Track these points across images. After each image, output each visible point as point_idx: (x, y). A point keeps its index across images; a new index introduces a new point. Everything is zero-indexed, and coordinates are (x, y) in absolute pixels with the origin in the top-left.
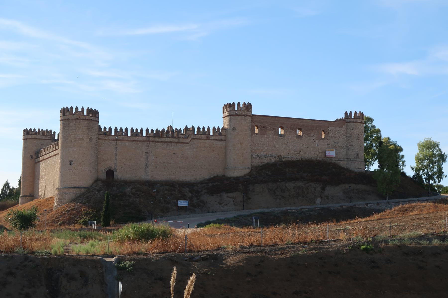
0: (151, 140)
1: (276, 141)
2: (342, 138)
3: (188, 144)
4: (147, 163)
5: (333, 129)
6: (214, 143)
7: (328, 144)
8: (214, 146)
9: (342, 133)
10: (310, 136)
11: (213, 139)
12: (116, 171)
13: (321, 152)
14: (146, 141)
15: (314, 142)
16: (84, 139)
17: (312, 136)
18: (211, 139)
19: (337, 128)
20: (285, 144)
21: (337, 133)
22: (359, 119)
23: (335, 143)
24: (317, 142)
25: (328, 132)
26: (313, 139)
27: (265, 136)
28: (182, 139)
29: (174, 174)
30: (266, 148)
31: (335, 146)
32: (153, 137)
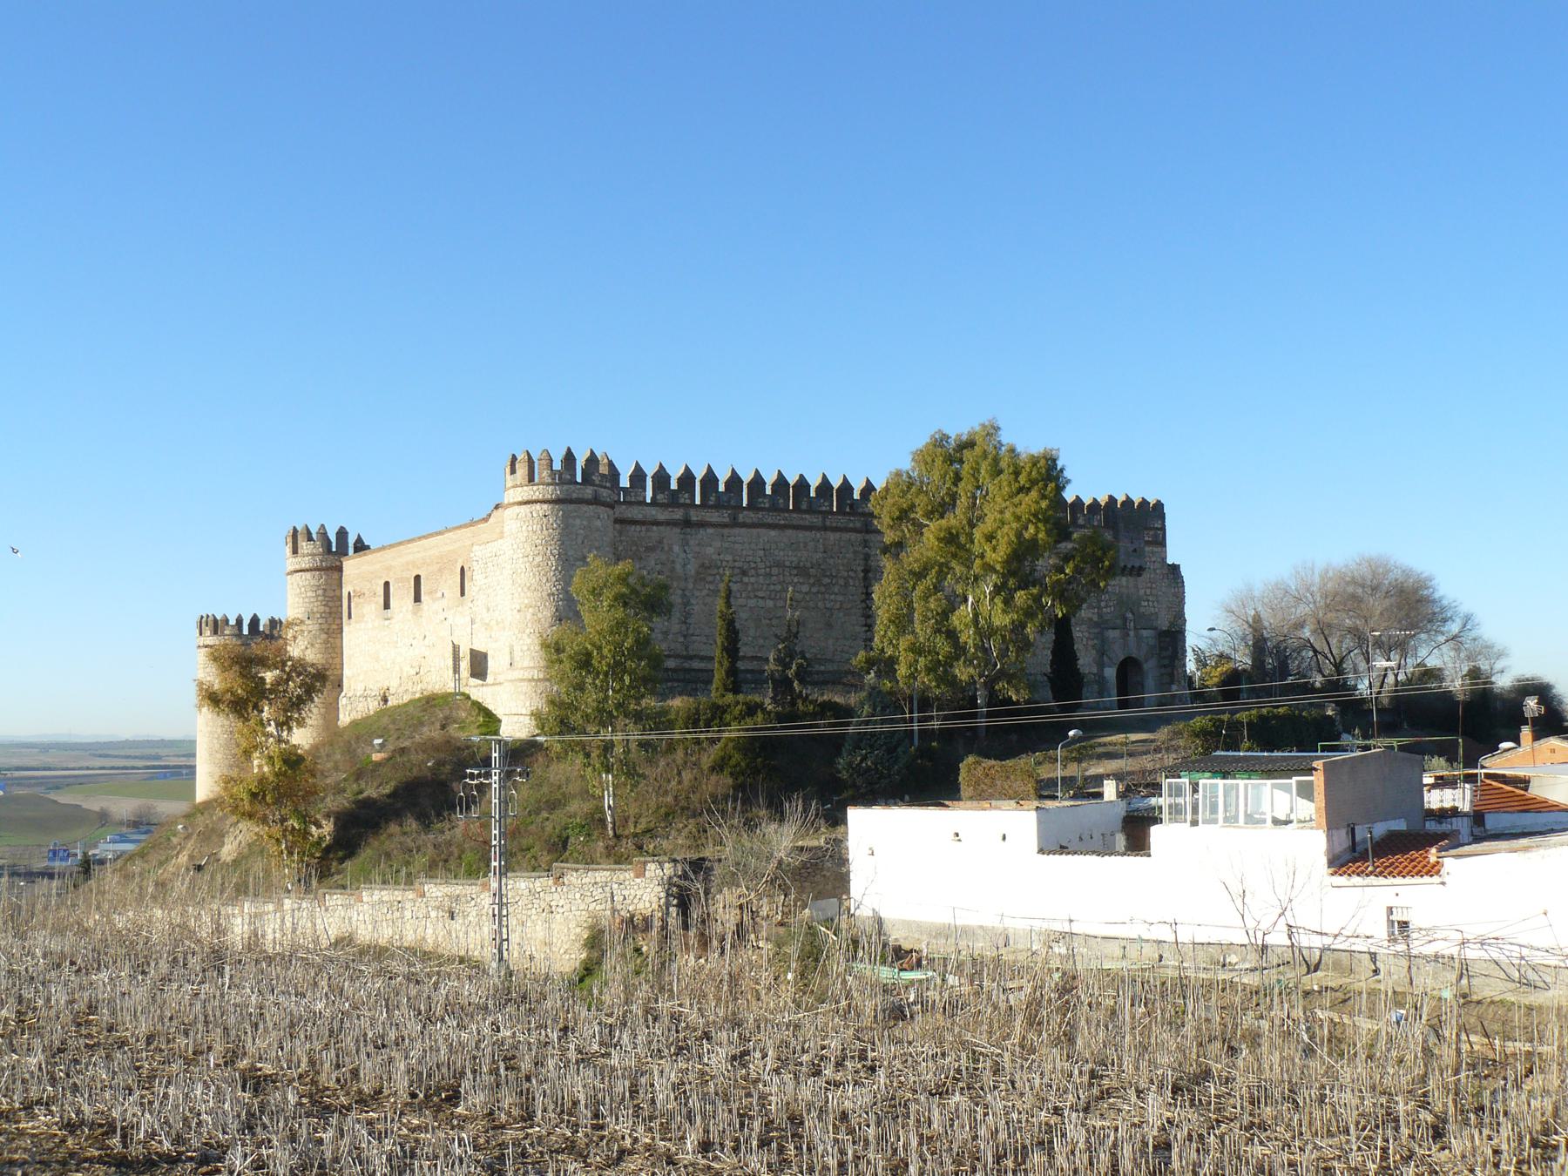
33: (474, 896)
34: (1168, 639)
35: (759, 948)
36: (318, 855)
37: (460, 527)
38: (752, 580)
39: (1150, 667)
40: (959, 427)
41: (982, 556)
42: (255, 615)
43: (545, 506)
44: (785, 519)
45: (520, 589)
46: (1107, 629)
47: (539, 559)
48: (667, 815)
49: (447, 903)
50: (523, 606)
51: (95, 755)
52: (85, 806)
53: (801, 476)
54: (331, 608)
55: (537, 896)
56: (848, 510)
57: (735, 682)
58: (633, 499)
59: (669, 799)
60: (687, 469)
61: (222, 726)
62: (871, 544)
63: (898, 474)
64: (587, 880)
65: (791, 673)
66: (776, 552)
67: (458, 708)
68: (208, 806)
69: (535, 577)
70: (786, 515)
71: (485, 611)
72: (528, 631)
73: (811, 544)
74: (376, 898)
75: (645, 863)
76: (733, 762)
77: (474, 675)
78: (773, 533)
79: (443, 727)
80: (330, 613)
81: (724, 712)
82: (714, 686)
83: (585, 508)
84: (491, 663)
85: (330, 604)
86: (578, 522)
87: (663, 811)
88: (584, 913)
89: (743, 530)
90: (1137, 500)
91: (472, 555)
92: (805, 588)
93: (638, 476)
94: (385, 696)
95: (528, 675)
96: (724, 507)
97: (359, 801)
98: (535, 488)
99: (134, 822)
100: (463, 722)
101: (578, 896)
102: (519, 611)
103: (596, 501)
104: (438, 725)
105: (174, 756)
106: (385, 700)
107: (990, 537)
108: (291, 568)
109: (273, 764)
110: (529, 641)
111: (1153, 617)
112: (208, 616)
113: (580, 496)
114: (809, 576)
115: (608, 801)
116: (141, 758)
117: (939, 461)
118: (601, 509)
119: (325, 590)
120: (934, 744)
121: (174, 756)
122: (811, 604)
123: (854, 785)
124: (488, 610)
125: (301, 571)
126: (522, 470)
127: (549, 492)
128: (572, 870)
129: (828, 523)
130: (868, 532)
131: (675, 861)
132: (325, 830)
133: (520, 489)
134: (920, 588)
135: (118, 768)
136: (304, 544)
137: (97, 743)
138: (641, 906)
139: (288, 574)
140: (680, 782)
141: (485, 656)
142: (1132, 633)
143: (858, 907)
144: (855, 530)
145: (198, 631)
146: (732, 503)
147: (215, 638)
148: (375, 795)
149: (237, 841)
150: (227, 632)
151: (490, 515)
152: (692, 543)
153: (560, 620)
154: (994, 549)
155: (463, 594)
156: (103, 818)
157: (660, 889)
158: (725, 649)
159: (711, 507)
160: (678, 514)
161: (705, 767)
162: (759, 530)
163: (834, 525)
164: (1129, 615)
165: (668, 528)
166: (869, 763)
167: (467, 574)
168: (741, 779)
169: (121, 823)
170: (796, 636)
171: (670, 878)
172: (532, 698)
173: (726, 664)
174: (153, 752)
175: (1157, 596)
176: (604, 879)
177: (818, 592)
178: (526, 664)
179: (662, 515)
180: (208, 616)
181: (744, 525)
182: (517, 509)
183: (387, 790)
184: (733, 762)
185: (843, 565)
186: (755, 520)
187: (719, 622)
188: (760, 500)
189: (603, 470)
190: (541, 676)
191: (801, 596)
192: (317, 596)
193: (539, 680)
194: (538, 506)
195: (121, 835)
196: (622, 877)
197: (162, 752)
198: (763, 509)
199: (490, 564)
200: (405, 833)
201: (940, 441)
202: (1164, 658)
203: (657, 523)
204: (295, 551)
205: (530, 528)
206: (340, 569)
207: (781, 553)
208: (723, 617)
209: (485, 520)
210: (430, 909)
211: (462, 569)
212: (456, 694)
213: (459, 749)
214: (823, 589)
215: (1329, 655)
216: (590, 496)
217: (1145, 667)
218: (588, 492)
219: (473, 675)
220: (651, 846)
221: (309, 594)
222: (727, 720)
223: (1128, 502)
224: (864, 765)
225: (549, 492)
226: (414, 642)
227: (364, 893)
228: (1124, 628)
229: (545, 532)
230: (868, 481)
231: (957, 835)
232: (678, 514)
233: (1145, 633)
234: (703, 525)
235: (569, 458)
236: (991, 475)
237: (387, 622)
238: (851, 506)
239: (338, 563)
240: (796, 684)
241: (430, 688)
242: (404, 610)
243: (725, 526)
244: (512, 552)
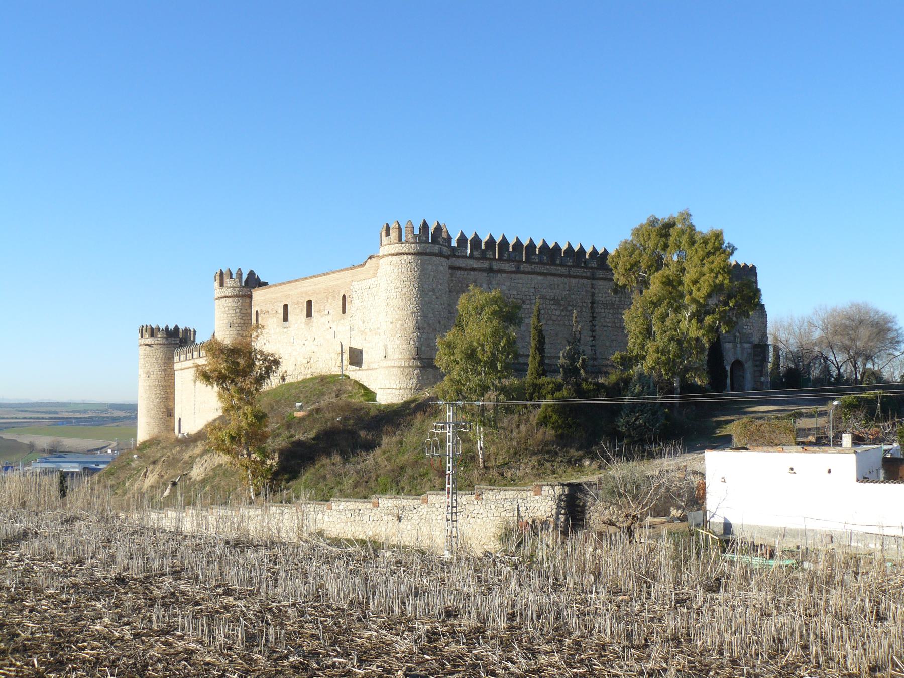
33: (416, 507)
34: (760, 349)
35: (641, 543)
36: (270, 477)
37: (343, 270)
38: (528, 307)
39: (749, 366)
40: (664, 215)
41: (690, 293)
42: (176, 326)
43: (410, 257)
44: (547, 269)
45: (392, 309)
46: (726, 342)
47: (405, 290)
48: (516, 453)
49: (396, 512)
50: (394, 320)
51: (19, 411)
52: (19, 440)
53: (556, 243)
54: (244, 321)
55: (463, 507)
56: (583, 265)
57: (544, 369)
58: (459, 254)
59: (515, 444)
60: (491, 236)
61: (156, 394)
62: (596, 287)
63: (626, 242)
64: (500, 497)
65: (579, 364)
66: (542, 290)
67: (346, 384)
68: (146, 445)
69: (402, 300)
70: (548, 267)
71: (361, 323)
72: (397, 336)
73: (562, 286)
74: (341, 507)
75: (542, 486)
76: (553, 420)
77: (352, 363)
78: (540, 278)
79: (337, 396)
80: (244, 324)
81: (540, 388)
82: (529, 372)
83: (434, 258)
84: (365, 356)
85: (244, 318)
86: (430, 267)
87: (512, 451)
88: (497, 518)
89: (523, 275)
90: (742, 265)
91: (352, 288)
92: (558, 313)
93: (462, 239)
94: (283, 376)
95: (397, 363)
96: (512, 261)
97: (294, 442)
98: (403, 245)
99: (50, 450)
100: (350, 392)
101: (493, 507)
102: (391, 323)
103: (440, 254)
104: (334, 395)
105: (66, 412)
106: (284, 379)
107: (695, 282)
108: (219, 295)
109: (246, 418)
110: (398, 342)
111: (750, 336)
112: (147, 326)
113: (432, 251)
114: (560, 305)
115: (480, 444)
116: (50, 413)
117: (653, 236)
118: (443, 259)
119: (241, 309)
120: (667, 410)
121: (66, 412)
122: (562, 323)
123: (630, 436)
124: (363, 323)
125: (225, 297)
126: (394, 234)
127: (412, 248)
128: (489, 490)
129: (571, 273)
130: (594, 279)
131: (563, 485)
132: (273, 462)
133: (393, 246)
134: (657, 313)
135: (34, 419)
136: (228, 280)
137: (20, 404)
138: (538, 514)
139: (217, 299)
140: (519, 433)
141: (361, 351)
142: (739, 345)
143: (713, 516)
144: (587, 278)
145: (140, 335)
146: (517, 258)
147: (151, 339)
148: (303, 439)
149: (204, 467)
150: (159, 336)
151: (365, 263)
152: (494, 282)
153: (419, 329)
154: (699, 290)
155: (344, 312)
156: (31, 447)
157: (552, 503)
158: (537, 348)
159: (505, 260)
160: (486, 265)
161: (535, 423)
162: (533, 276)
163: (575, 274)
164: (737, 334)
165: (480, 273)
166: (641, 421)
167: (348, 300)
168: (560, 432)
169: (43, 451)
170: (579, 341)
171: (560, 496)
172: (400, 379)
173: (538, 358)
174: (53, 409)
175: (752, 323)
176: (512, 496)
177: (565, 316)
178: (396, 357)
179: (476, 264)
180: (147, 326)
181: (524, 273)
182: (390, 258)
183: (312, 435)
184: (553, 420)
185: (579, 299)
186: (530, 270)
187: (533, 332)
188: (533, 257)
189: (445, 235)
190: (407, 364)
191: (556, 317)
192: (236, 313)
193: (405, 367)
194: (405, 257)
195: (45, 458)
196: (524, 495)
197: (58, 409)
198: (534, 263)
199: (365, 294)
200: (334, 464)
201: (653, 222)
202: (757, 360)
203: (473, 269)
204: (222, 285)
205: (400, 270)
206: (250, 297)
207: (545, 290)
208: (536, 328)
209: (362, 265)
210: (383, 515)
211: (344, 297)
212: (340, 375)
213: (356, 409)
214: (568, 314)
215: (834, 361)
216: (437, 251)
217: (746, 365)
218: (436, 248)
219: (351, 363)
220: (509, 474)
221: (230, 312)
222: (544, 394)
223: (746, 266)
224: (637, 423)
225: (412, 248)
226: (306, 343)
227: (333, 504)
228: (734, 342)
229: (409, 273)
230: (594, 247)
231: (792, 469)
232: (486, 265)
233: (746, 345)
234: (500, 271)
235: (425, 226)
236: (689, 244)
237: (285, 330)
238: (585, 263)
239: (249, 293)
240: (582, 371)
241: (318, 371)
242: (299, 322)
243: (512, 272)
244: (387, 285)
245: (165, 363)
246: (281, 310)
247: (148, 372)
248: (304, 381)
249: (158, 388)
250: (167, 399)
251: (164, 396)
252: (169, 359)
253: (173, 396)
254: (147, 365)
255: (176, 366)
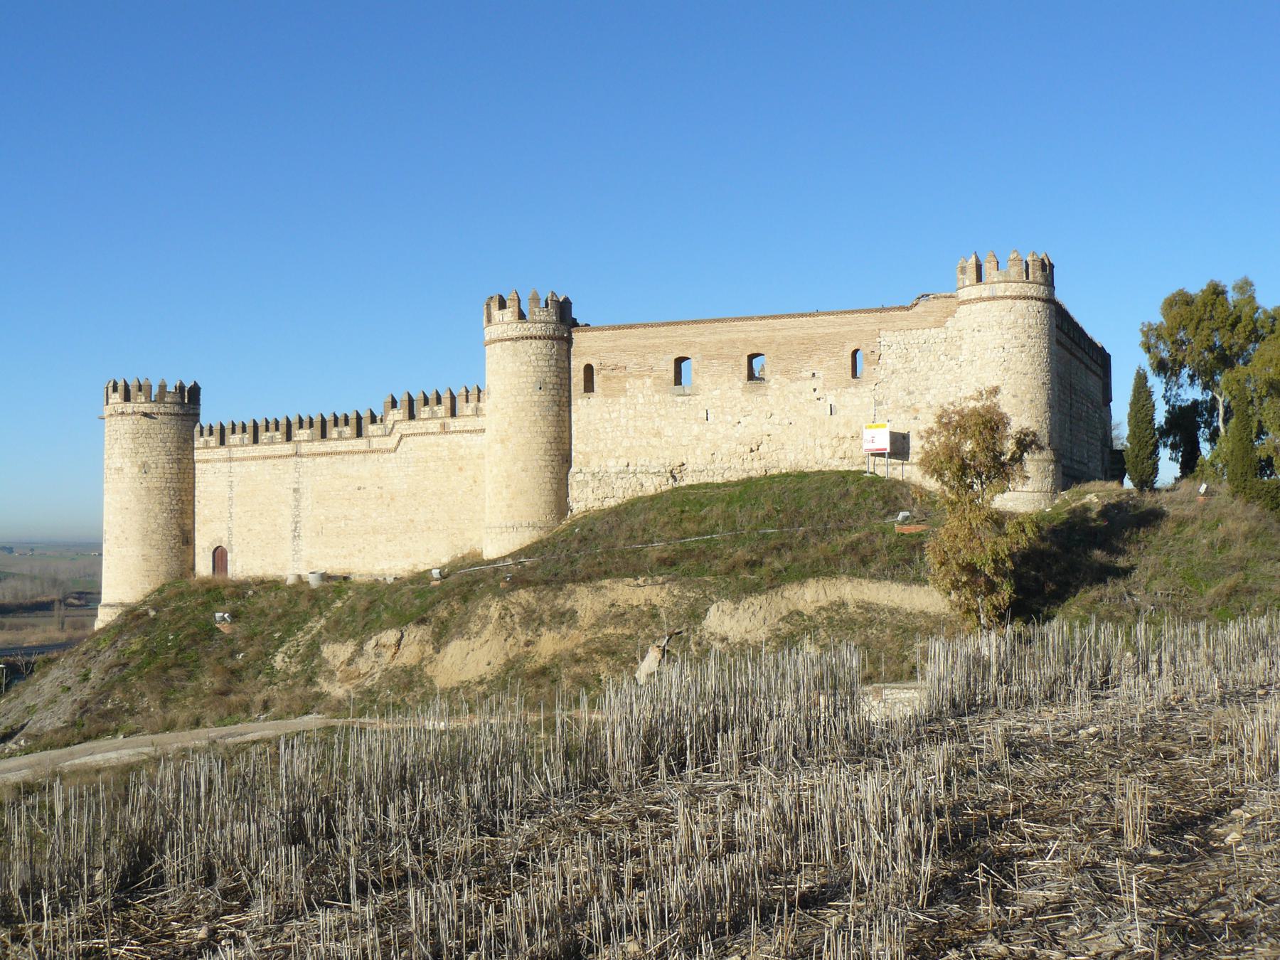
0: (303, 451)
1: (663, 412)
2: (941, 372)
3: (393, 455)
4: (297, 522)
5: (899, 338)
6: (463, 443)
7: (878, 403)
8: (461, 452)
9: (943, 348)
10: (798, 379)
11: (458, 429)
12: (232, 552)
13: (849, 435)
14: (291, 456)
15: (819, 399)
16: (125, 471)
17: (806, 379)
18: (452, 429)
19: (920, 332)
20: (696, 420)
21: (919, 355)
22: (1005, 282)
23: (910, 393)
24: (831, 399)
25: (877, 352)
26: (815, 390)
27: (622, 400)
28: (377, 439)
29: (360, 551)
30: (626, 443)
31: (912, 404)
32: (308, 441)
98: (1030, 285)
206: (569, 341)
221: (541, 363)
245: (178, 448)
246: (848, 362)
247: (144, 464)
248: (725, 485)
249: (165, 492)
250: (182, 512)
251: (176, 507)
252: (186, 441)
253: (191, 507)
254: (141, 450)
255: (198, 455)
